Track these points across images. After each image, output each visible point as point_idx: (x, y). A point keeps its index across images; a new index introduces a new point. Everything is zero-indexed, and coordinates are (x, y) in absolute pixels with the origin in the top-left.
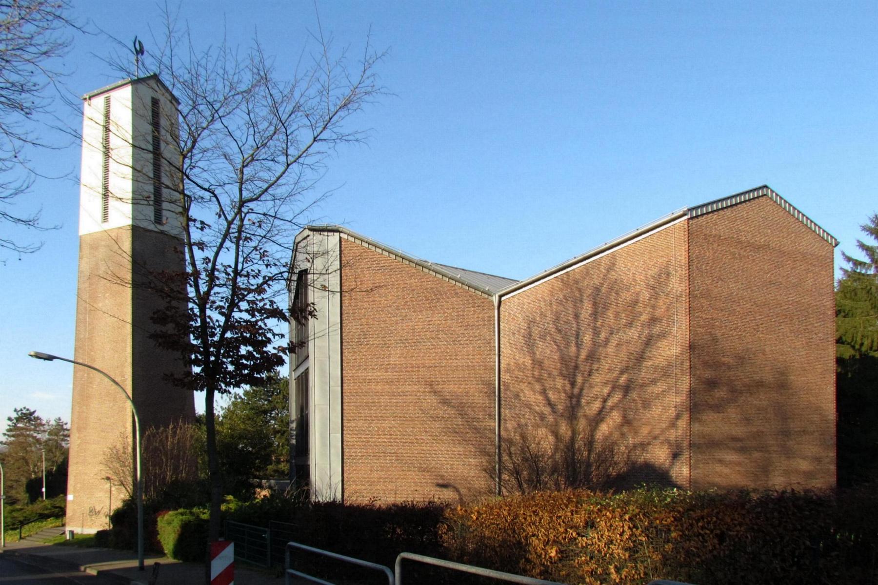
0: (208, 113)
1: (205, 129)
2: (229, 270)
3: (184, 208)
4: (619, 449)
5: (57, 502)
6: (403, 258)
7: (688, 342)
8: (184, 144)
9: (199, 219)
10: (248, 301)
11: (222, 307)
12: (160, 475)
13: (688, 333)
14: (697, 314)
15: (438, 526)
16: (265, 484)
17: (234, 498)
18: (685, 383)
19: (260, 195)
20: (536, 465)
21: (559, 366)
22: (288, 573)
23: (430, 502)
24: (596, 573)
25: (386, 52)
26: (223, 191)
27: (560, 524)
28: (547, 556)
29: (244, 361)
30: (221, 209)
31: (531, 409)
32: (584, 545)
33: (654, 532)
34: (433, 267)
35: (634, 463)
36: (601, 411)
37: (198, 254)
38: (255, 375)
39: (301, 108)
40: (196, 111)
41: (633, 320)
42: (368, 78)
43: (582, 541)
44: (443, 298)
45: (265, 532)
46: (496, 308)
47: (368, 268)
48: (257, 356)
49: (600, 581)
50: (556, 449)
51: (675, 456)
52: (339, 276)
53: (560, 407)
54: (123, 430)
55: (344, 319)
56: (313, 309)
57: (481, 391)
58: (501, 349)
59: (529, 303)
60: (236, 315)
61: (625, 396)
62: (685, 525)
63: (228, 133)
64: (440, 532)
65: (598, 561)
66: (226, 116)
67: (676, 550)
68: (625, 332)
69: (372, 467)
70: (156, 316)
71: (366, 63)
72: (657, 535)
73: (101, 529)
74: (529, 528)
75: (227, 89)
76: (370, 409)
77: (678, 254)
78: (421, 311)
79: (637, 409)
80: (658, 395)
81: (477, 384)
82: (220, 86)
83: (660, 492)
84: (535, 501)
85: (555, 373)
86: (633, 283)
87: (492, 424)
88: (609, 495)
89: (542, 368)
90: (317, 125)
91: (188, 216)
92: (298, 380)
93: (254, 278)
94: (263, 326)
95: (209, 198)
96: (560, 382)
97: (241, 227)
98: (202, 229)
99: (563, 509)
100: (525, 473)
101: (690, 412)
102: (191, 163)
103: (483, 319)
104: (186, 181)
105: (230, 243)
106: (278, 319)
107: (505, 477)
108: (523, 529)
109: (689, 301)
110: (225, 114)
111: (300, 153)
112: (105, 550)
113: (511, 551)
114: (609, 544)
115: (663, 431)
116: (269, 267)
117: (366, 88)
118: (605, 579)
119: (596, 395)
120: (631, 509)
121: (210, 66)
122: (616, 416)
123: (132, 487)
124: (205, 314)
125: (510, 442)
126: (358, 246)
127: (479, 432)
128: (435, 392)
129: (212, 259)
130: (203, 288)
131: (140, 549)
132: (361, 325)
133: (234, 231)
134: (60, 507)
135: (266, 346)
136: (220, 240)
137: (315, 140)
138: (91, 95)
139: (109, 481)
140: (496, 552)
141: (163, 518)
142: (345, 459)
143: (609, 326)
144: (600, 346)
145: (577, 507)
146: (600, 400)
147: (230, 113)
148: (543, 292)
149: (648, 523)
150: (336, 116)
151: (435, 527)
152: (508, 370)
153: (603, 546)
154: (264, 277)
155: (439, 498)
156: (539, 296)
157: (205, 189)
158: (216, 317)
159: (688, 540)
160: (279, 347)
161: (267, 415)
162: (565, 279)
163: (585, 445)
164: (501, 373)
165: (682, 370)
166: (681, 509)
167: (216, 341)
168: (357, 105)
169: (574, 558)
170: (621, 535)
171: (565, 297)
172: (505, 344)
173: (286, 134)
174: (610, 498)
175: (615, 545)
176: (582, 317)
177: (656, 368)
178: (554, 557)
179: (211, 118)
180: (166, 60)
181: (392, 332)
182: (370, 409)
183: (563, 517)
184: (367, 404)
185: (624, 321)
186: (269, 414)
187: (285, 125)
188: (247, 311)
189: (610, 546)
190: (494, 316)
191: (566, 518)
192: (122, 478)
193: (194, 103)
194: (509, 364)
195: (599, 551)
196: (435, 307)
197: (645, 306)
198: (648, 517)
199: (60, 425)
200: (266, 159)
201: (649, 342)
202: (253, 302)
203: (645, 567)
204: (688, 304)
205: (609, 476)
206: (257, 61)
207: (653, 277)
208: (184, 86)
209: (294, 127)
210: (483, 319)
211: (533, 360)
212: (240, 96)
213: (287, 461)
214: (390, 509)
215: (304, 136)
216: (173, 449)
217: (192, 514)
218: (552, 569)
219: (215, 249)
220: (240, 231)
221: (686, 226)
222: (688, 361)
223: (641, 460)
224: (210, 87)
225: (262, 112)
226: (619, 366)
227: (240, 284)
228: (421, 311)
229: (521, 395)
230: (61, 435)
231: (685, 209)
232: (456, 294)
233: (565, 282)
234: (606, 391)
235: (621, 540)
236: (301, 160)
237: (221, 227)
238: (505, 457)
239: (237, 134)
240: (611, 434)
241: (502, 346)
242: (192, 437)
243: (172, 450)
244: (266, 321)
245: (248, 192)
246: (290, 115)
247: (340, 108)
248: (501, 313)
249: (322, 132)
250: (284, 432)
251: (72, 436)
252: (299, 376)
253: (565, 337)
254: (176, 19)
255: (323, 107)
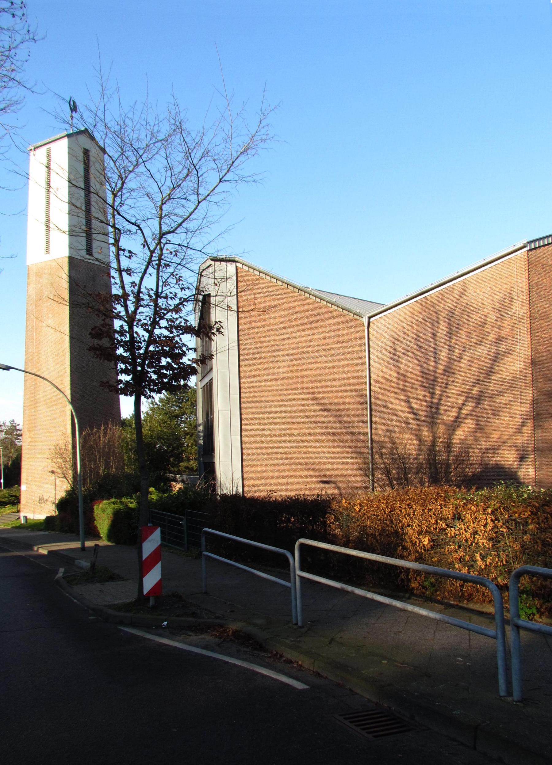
0: (133, 159)
1: (131, 172)
2: (152, 293)
3: (115, 239)
4: (474, 452)
5: (13, 490)
6: (288, 285)
7: (530, 358)
8: (114, 184)
9: (127, 248)
10: (167, 320)
11: (146, 324)
12: (94, 469)
13: (530, 350)
14: (537, 334)
15: (326, 516)
16: (179, 478)
17: (155, 490)
18: (528, 394)
19: (176, 228)
20: (404, 465)
21: (420, 379)
22: (205, 555)
23: (318, 495)
24: (464, 559)
25: (278, 105)
26: (146, 225)
27: (431, 516)
28: (421, 544)
29: (165, 372)
30: (146, 241)
31: (397, 416)
32: (453, 535)
33: (513, 524)
34: (313, 292)
35: (487, 465)
36: (456, 419)
37: (127, 279)
38: (174, 383)
39: (210, 154)
40: (124, 157)
41: (483, 338)
42: (263, 127)
43: (451, 532)
44: (322, 319)
45: (182, 520)
46: (366, 328)
47: (260, 293)
48: (175, 366)
49: (468, 567)
50: (420, 450)
51: (522, 458)
52: (236, 300)
53: (422, 414)
54: (64, 430)
55: (241, 337)
56: (220, 326)
57: (356, 400)
58: (371, 363)
59: (394, 324)
60: (157, 331)
61: (477, 405)
62: (541, 518)
63: (150, 176)
64: (329, 522)
65: (466, 550)
66: (148, 160)
67: (533, 540)
68: (476, 350)
69: (266, 465)
70: (94, 332)
71: (262, 115)
72: (516, 528)
73: (49, 515)
74: (405, 519)
75: (148, 139)
76: (264, 415)
77: (520, 281)
78: (304, 330)
79: (488, 417)
80: (506, 404)
81: (352, 394)
82: (143, 136)
83: (516, 489)
84: (408, 496)
85: (417, 384)
86: (482, 306)
87: (365, 429)
88: (472, 491)
89: (406, 380)
90: (223, 168)
91: (118, 245)
92: (204, 389)
93: (172, 300)
94: (179, 341)
95: (135, 231)
96: (421, 393)
97: (161, 254)
98: (130, 258)
99: (434, 503)
100: (394, 472)
101: (534, 420)
102: (121, 201)
103: (356, 338)
104: (117, 216)
105: (153, 269)
106: (192, 335)
107: (378, 475)
108: (399, 520)
109: (530, 323)
110: (148, 159)
111: (209, 192)
112: (54, 532)
113: (389, 539)
114: (475, 535)
115: (511, 437)
116: (183, 290)
117: (262, 136)
118: (472, 566)
119: (453, 404)
120: (493, 503)
121: (136, 119)
122: (469, 424)
123: (72, 479)
124: (133, 330)
125: (381, 445)
126: (251, 274)
127: (354, 435)
128: (317, 401)
129: (138, 283)
130: (131, 308)
131: (81, 533)
132: (255, 342)
133: (155, 259)
134: (15, 496)
135: (181, 358)
136: (144, 267)
137: (220, 181)
138: (35, 146)
139: (54, 474)
140: (377, 541)
141: (98, 506)
142: (244, 457)
143: (463, 344)
144: (455, 361)
145: (445, 501)
146: (456, 409)
147: (151, 158)
148: (405, 314)
149: (508, 516)
150: (237, 160)
151: (324, 517)
152: (377, 382)
153: (469, 536)
154: (180, 299)
155: (326, 492)
156: (402, 318)
157: (132, 224)
158: (141, 333)
159: (544, 532)
160: (193, 359)
161: (178, 419)
162: (424, 303)
163: (445, 448)
164: (372, 385)
165: (526, 383)
166: (537, 505)
167: (142, 354)
168: (254, 151)
169: (444, 546)
170: (485, 526)
171: (423, 318)
172: (374, 359)
173: (198, 176)
174: (474, 493)
175: (480, 536)
176: (439, 335)
177: (503, 381)
178: (427, 545)
179: (136, 163)
180: (100, 114)
181: (280, 348)
182: (264, 415)
183: (433, 510)
184: (261, 410)
185: (474, 340)
186: (180, 419)
187: (197, 167)
188: (166, 328)
189: (476, 536)
190: (364, 335)
191: (436, 511)
192: (65, 472)
193: (122, 149)
194: (378, 376)
195: (466, 541)
196: (315, 327)
197: (493, 326)
198: (507, 511)
199: (13, 426)
200: (180, 198)
201: (496, 358)
202: (172, 320)
203: (507, 556)
204: (529, 325)
205: (465, 476)
206: (173, 112)
207: (499, 302)
208: (115, 135)
209: (204, 169)
210: (356, 338)
211: (398, 373)
212: (159, 144)
213: (196, 459)
214: (285, 500)
215: (212, 178)
216: (104, 447)
217: (121, 502)
218: (425, 555)
219: (140, 275)
220: (160, 259)
221: (526, 257)
222: (530, 375)
223: (492, 462)
224: (135, 136)
225: (178, 157)
226: (472, 379)
227: (160, 304)
228: (304, 330)
229: (389, 403)
230: (14, 435)
231: (525, 242)
232: (333, 315)
233: (424, 306)
234: (461, 400)
235: (485, 531)
236: (208, 198)
237: (145, 255)
238: (377, 458)
239: (157, 176)
240: (466, 438)
241: (372, 360)
242: (119, 437)
243: (103, 448)
244: (181, 336)
245: (166, 226)
246: (200, 160)
247: (241, 154)
248: (370, 332)
249: (226, 174)
250: (193, 434)
251: (24, 435)
252: (204, 386)
253: (425, 354)
254: (108, 79)
255: (227, 153)
